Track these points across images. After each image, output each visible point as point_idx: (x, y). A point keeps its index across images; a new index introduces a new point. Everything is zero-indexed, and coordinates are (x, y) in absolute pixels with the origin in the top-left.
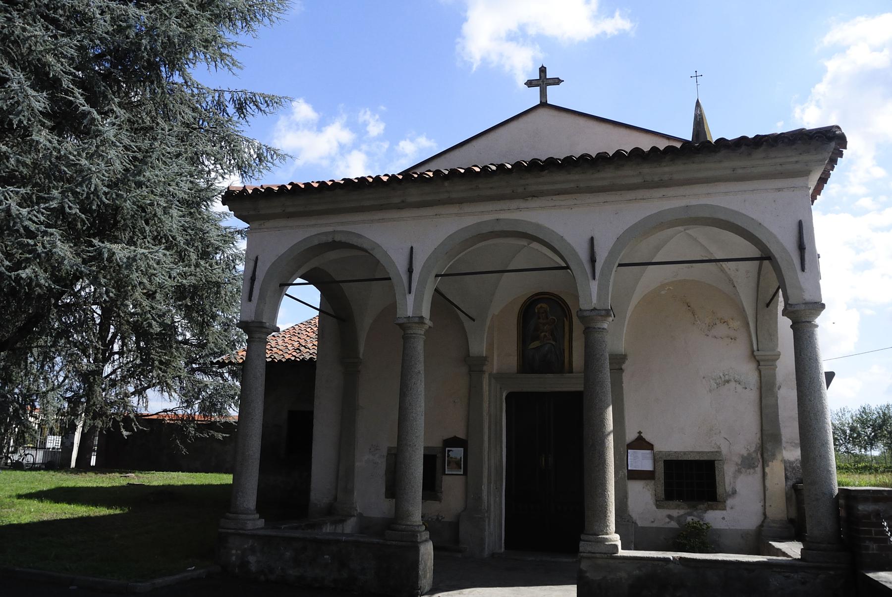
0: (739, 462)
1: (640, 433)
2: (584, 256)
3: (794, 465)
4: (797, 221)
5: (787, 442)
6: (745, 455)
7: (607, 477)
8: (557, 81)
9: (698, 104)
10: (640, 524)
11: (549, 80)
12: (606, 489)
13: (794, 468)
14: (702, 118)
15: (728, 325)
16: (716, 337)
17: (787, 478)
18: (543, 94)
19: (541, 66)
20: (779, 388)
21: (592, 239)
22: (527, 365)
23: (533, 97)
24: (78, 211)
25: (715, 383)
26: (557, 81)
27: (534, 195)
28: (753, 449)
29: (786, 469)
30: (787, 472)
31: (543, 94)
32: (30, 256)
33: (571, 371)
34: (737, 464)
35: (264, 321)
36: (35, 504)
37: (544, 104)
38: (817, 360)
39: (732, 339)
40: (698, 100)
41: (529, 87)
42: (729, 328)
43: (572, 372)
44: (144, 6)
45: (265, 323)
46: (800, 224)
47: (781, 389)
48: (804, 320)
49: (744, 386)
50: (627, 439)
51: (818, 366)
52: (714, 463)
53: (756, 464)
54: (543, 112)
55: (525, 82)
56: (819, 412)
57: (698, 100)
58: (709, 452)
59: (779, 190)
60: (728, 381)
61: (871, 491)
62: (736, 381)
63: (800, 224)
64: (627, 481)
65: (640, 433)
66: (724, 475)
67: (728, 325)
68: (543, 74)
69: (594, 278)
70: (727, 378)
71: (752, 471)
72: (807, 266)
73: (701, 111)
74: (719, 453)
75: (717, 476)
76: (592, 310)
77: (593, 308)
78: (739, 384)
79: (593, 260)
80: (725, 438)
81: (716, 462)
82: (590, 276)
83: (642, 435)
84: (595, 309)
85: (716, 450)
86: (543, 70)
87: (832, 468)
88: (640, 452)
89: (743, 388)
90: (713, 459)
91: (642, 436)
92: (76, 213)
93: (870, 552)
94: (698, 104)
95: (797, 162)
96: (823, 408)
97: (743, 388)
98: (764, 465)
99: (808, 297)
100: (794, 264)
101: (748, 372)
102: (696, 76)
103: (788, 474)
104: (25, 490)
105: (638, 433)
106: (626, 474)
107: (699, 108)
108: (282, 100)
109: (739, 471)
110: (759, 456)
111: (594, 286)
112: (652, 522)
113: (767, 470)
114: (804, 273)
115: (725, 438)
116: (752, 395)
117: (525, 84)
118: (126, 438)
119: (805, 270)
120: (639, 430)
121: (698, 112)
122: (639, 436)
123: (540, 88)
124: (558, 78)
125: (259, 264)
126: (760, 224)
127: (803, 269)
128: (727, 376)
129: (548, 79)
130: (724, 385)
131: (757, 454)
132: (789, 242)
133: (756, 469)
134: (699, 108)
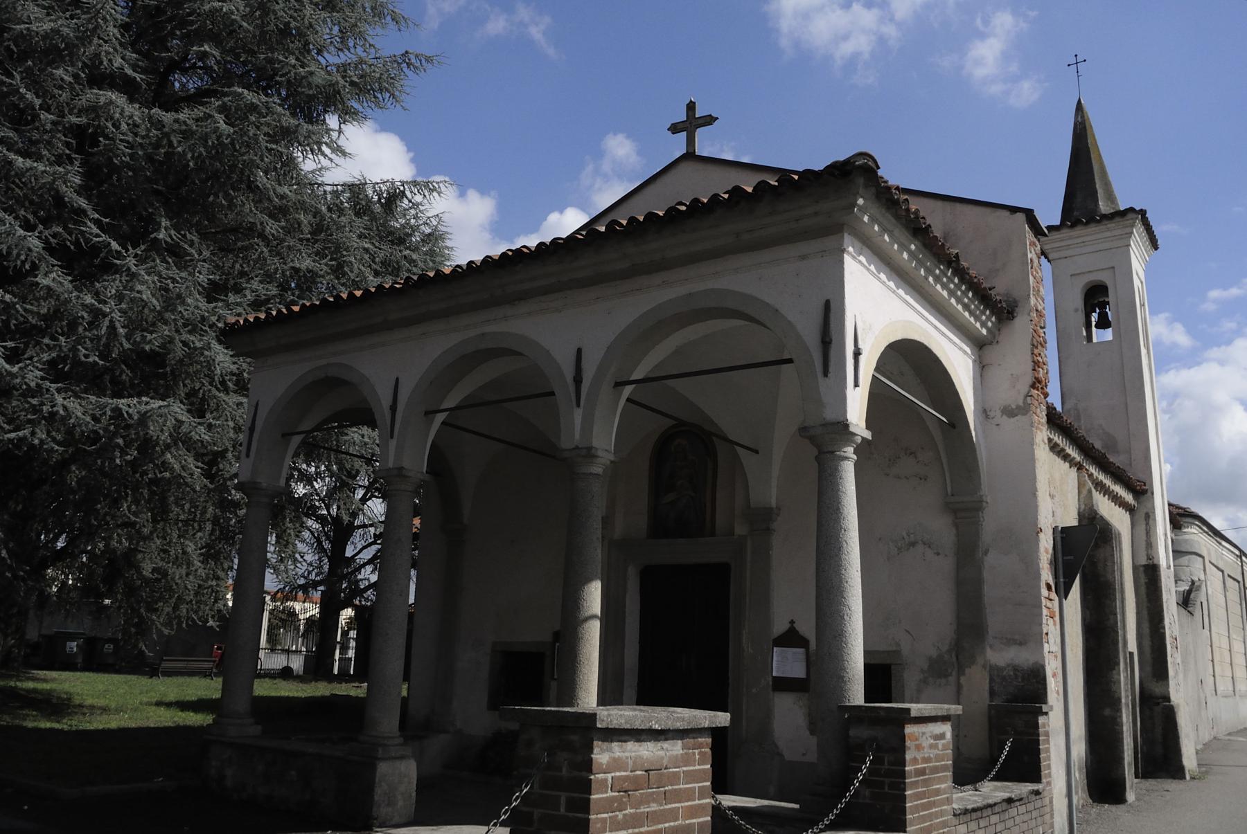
0: (926, 667)
1: (792, 622)
2: (569, 374)
3: (1005, 673)
4: (823, 302)
5: (996, 638)
6: (935, 656)
7: (578, 679)
8: (709, 120)
9: (1079, 106)
10: (788, 756)
11: (699, 120)
12: (575, 696)
13: (1004, 678)
14: (1085, 127)
15: (916, 457)
16: (899, 478)
17: (992, 693)
18: (691, 141)
19: (688, 102)
20: (986, 552)
21: (579, 351)
22: (661, 527)
23: (678, 147)
24: (97, 359)
25: (896, 547)
26: (709, 120)
27: (523, 297)
28: (945, 648)
29: (991, 680)
30: (993, 685)
31: (691, 141)
32: (35, 417)
33: (713, 534)
34: (922, 671)
35: (259, 481)
36: (162, 710)
37: (690, 156)
38: (838, 509)
39: (921, 479)
40: (1079, 101)
41: (673, 133)
42: (918, 462)
43: (713, 534)
44: (207, 103)
45: (260, 483)
46: (827, 305)
47: (989, 555)
48: (826, 450)
49: (935, 551)
50: (775, 631)
51: (839, 518)
52: (890, 667)
53: (950, 671)
54: (687, 168)
55: (669, 127)
56: (833, 588)
57: (1079, 101)
58: (883, 652)
59: (803, 257)
60: (913, 544)
61: (863, 708)
62: (925, 544)
63: (827, 305)
64: (771, 693)
65: (792, 622)
66: (903, 687)
67: (916, 457)
68: (690, 113)
69: (578, 405)
70: (912, 538)
71: (943, 681)
72: (831, 369)
73: (1083, 117)
74: (897, 653)
75: (893, 688)
76: (574, 449)
77: (573, 446)
78: (930, 547)
79: (578, 380)
80: (907, 631)
81: (892, 667)
82: (574, 403)
83: (795, 625)
84: (577, 448)
85: (894, 649)
86: (691, 107)
87: (847, 673)
88: (791, 651)
89: (935, 553)
90: (888, 662)
91: (795, 628)
92: (94, 361)
93: (861, 801)
94: (1079, 106)
95: (816, 214)
96: (841, 581)
97: (935, 553)
98: (961, 671)
99: (829, 415)
100: (815, 366)
101: (941, 528)
102: (1077, 63)
103: (996, 688)
104: (172, 697)
105: (790, 623)
106: (771, 683)
107: (1080, 113)
108: (441, 185)
109: (925, 681)
110: (954, 659)
111: (578, 415)
112: (804, 755)
113: (963, 679)
114: (827, 379)
115: (907, 631)
116: (945, 564)
117: (668, 130)
118: (218, 630)
119: (829, 375)
120: (791, 618)
121: (1079, 119)
122: (790, 628)
123: (687, 133)
124: (710, 115)
125: (259, 408)
126: (777, 310)
127: (826, 373)
128: (912, 536)
129: (698, 118)
130: (908, 549)
131: (951, 656)
132: (809, 333)
133: (950, 678)
134: (1080, 113)
